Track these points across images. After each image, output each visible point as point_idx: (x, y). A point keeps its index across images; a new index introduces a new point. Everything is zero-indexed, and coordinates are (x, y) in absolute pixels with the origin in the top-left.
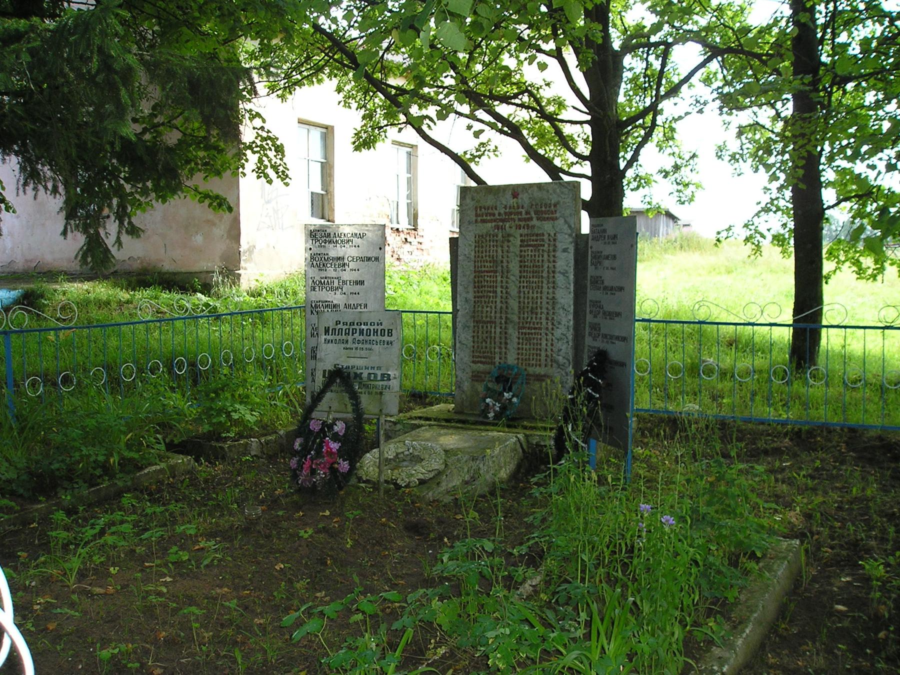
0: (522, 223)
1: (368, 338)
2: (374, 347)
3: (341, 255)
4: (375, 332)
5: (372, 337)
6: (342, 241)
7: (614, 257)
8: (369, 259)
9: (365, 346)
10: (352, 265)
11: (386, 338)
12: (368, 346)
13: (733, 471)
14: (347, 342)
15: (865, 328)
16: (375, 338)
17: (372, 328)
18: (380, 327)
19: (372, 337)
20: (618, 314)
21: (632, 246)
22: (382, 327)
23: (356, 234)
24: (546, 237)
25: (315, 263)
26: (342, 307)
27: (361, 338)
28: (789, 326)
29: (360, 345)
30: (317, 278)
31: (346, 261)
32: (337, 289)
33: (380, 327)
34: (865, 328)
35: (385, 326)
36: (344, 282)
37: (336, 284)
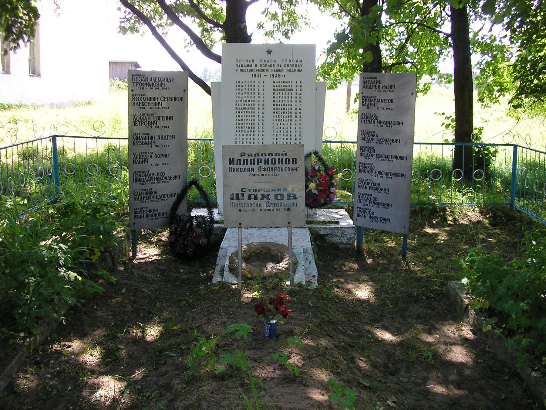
0: (275, 73)
1: (274, 166)
2: (280, 173)
3: (155, 95)
4: (281, 161)
5: (277, 165)
6: (156, 84)
7: (392, 101)
8: (176, 99)
9: (270, 173)
10: (164, 104)
11: (291, 166)
12: (273, 172)
13: (345, 238)
14: (253, 170)
15: (87, 138)
16: (280, 166)
17: (277, 158)
18: (284, 158)
19: (277, 165)
20: (395, 141)
21: (185, 91)
22: (286, 157)
23: (167, 79)
24: (294, 84)
25: (136, 102)
26: (156, 138)
27: (267, 166)
28: (127, 139)
29: (266, 172)
30: (138, 115)
31: (159, 101)
32: (152, 124)
33: (284, 158)
34: (87, 138)
35: (290, 156)
36: (158, 118)
37: (152, 120)
